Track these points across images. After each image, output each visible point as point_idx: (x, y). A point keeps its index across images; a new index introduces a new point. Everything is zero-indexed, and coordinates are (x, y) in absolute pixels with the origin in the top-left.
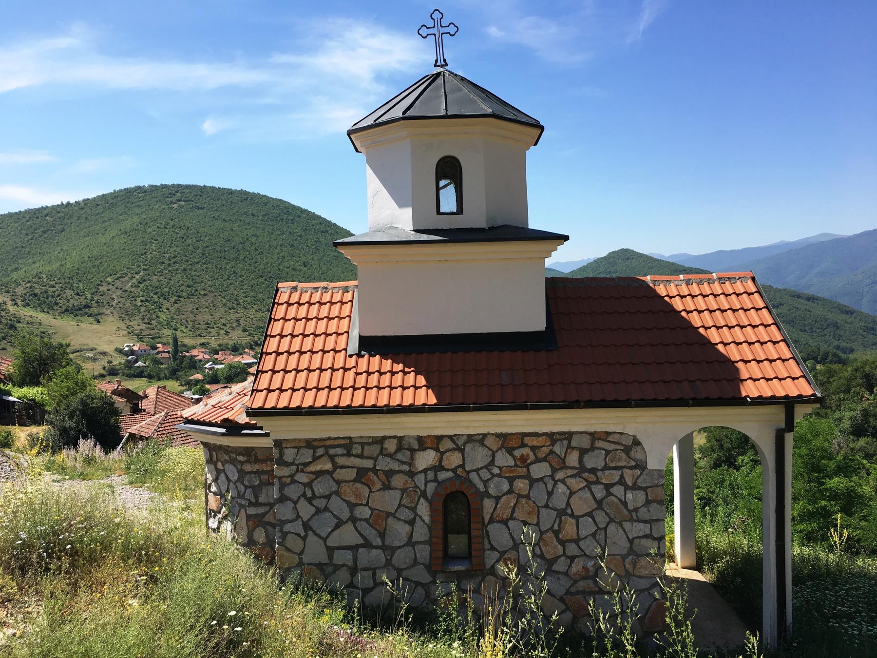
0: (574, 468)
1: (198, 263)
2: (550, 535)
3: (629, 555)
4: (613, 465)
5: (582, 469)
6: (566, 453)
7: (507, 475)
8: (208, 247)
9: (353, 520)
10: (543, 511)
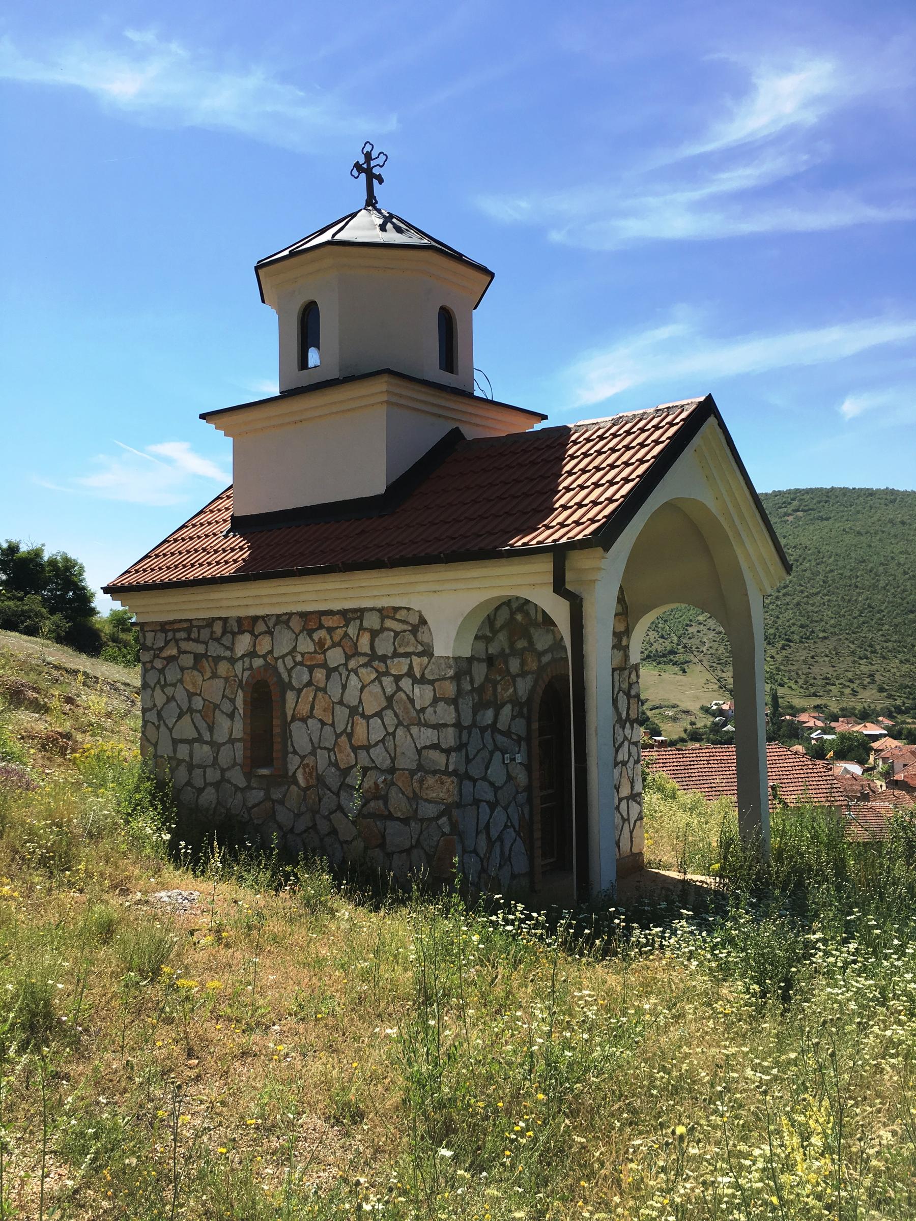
0: (365, 654)
1: (817, 594)
2: (344, 738)
3: (419, 771)
4: (401, 650)
5: (373, 656)
6: (358, 637)
7: (309, 663)
8: (832, 571)
9: (191, 710)
10: (337, 707)
